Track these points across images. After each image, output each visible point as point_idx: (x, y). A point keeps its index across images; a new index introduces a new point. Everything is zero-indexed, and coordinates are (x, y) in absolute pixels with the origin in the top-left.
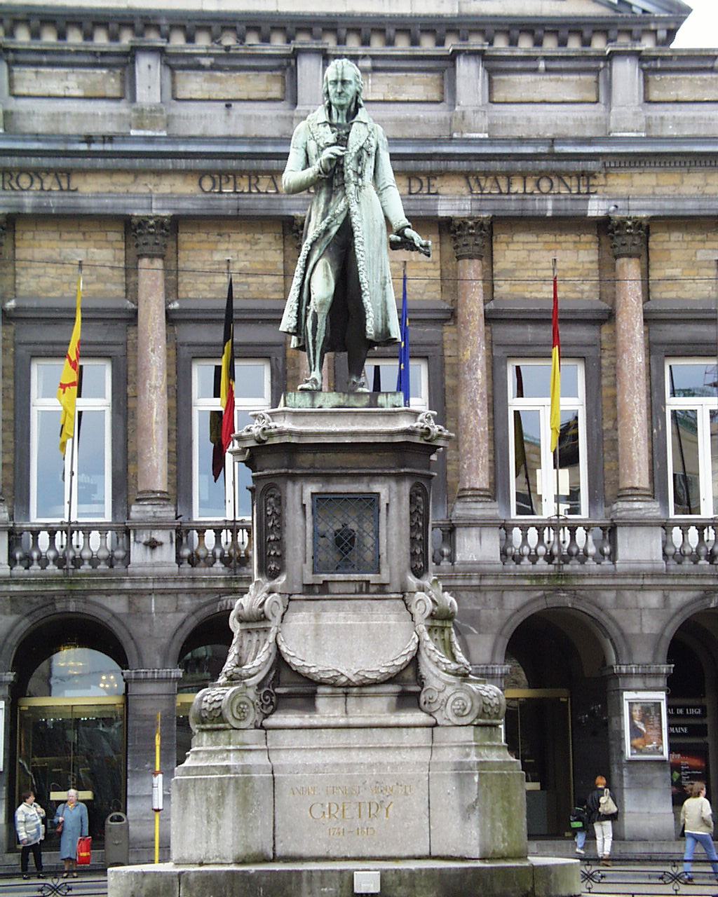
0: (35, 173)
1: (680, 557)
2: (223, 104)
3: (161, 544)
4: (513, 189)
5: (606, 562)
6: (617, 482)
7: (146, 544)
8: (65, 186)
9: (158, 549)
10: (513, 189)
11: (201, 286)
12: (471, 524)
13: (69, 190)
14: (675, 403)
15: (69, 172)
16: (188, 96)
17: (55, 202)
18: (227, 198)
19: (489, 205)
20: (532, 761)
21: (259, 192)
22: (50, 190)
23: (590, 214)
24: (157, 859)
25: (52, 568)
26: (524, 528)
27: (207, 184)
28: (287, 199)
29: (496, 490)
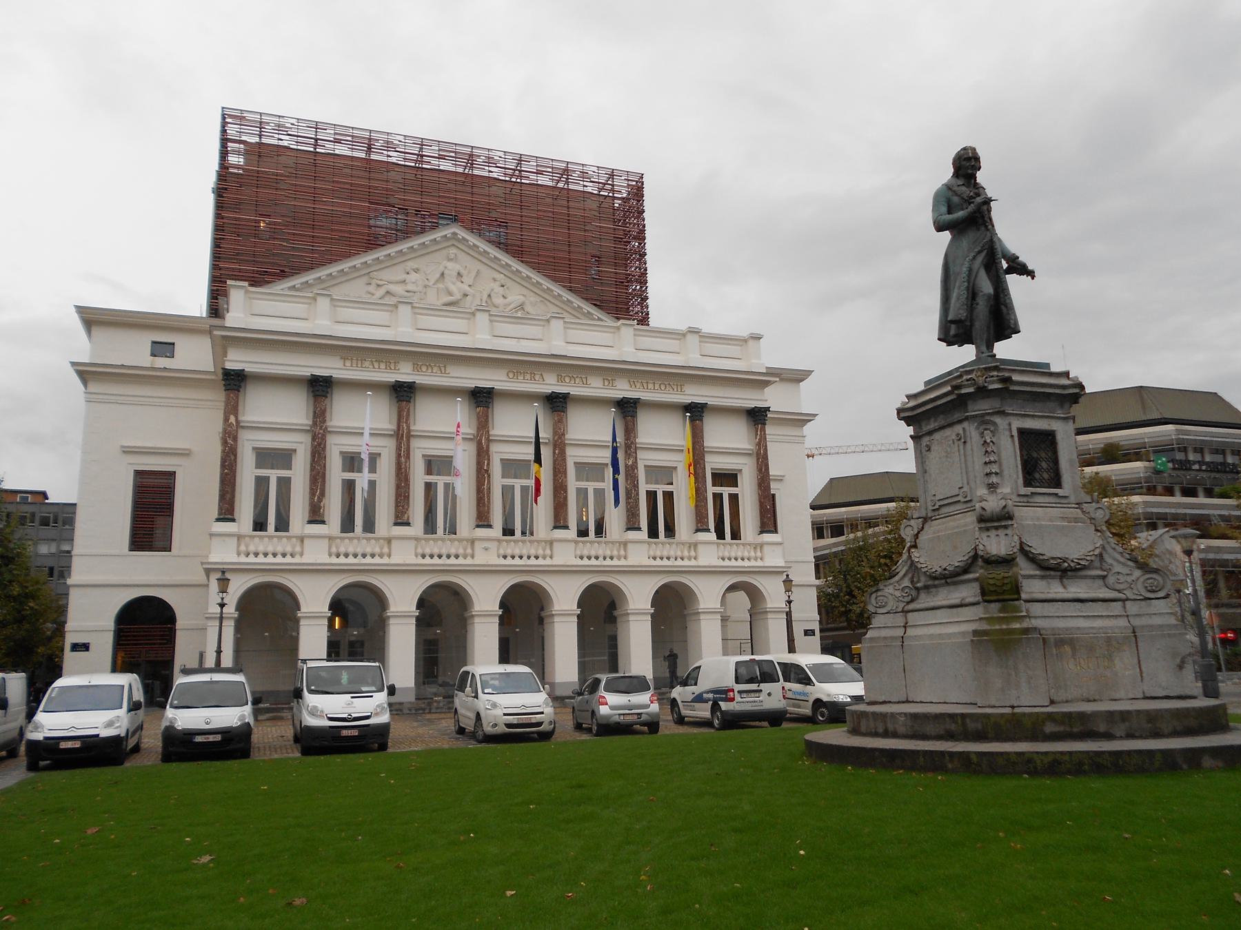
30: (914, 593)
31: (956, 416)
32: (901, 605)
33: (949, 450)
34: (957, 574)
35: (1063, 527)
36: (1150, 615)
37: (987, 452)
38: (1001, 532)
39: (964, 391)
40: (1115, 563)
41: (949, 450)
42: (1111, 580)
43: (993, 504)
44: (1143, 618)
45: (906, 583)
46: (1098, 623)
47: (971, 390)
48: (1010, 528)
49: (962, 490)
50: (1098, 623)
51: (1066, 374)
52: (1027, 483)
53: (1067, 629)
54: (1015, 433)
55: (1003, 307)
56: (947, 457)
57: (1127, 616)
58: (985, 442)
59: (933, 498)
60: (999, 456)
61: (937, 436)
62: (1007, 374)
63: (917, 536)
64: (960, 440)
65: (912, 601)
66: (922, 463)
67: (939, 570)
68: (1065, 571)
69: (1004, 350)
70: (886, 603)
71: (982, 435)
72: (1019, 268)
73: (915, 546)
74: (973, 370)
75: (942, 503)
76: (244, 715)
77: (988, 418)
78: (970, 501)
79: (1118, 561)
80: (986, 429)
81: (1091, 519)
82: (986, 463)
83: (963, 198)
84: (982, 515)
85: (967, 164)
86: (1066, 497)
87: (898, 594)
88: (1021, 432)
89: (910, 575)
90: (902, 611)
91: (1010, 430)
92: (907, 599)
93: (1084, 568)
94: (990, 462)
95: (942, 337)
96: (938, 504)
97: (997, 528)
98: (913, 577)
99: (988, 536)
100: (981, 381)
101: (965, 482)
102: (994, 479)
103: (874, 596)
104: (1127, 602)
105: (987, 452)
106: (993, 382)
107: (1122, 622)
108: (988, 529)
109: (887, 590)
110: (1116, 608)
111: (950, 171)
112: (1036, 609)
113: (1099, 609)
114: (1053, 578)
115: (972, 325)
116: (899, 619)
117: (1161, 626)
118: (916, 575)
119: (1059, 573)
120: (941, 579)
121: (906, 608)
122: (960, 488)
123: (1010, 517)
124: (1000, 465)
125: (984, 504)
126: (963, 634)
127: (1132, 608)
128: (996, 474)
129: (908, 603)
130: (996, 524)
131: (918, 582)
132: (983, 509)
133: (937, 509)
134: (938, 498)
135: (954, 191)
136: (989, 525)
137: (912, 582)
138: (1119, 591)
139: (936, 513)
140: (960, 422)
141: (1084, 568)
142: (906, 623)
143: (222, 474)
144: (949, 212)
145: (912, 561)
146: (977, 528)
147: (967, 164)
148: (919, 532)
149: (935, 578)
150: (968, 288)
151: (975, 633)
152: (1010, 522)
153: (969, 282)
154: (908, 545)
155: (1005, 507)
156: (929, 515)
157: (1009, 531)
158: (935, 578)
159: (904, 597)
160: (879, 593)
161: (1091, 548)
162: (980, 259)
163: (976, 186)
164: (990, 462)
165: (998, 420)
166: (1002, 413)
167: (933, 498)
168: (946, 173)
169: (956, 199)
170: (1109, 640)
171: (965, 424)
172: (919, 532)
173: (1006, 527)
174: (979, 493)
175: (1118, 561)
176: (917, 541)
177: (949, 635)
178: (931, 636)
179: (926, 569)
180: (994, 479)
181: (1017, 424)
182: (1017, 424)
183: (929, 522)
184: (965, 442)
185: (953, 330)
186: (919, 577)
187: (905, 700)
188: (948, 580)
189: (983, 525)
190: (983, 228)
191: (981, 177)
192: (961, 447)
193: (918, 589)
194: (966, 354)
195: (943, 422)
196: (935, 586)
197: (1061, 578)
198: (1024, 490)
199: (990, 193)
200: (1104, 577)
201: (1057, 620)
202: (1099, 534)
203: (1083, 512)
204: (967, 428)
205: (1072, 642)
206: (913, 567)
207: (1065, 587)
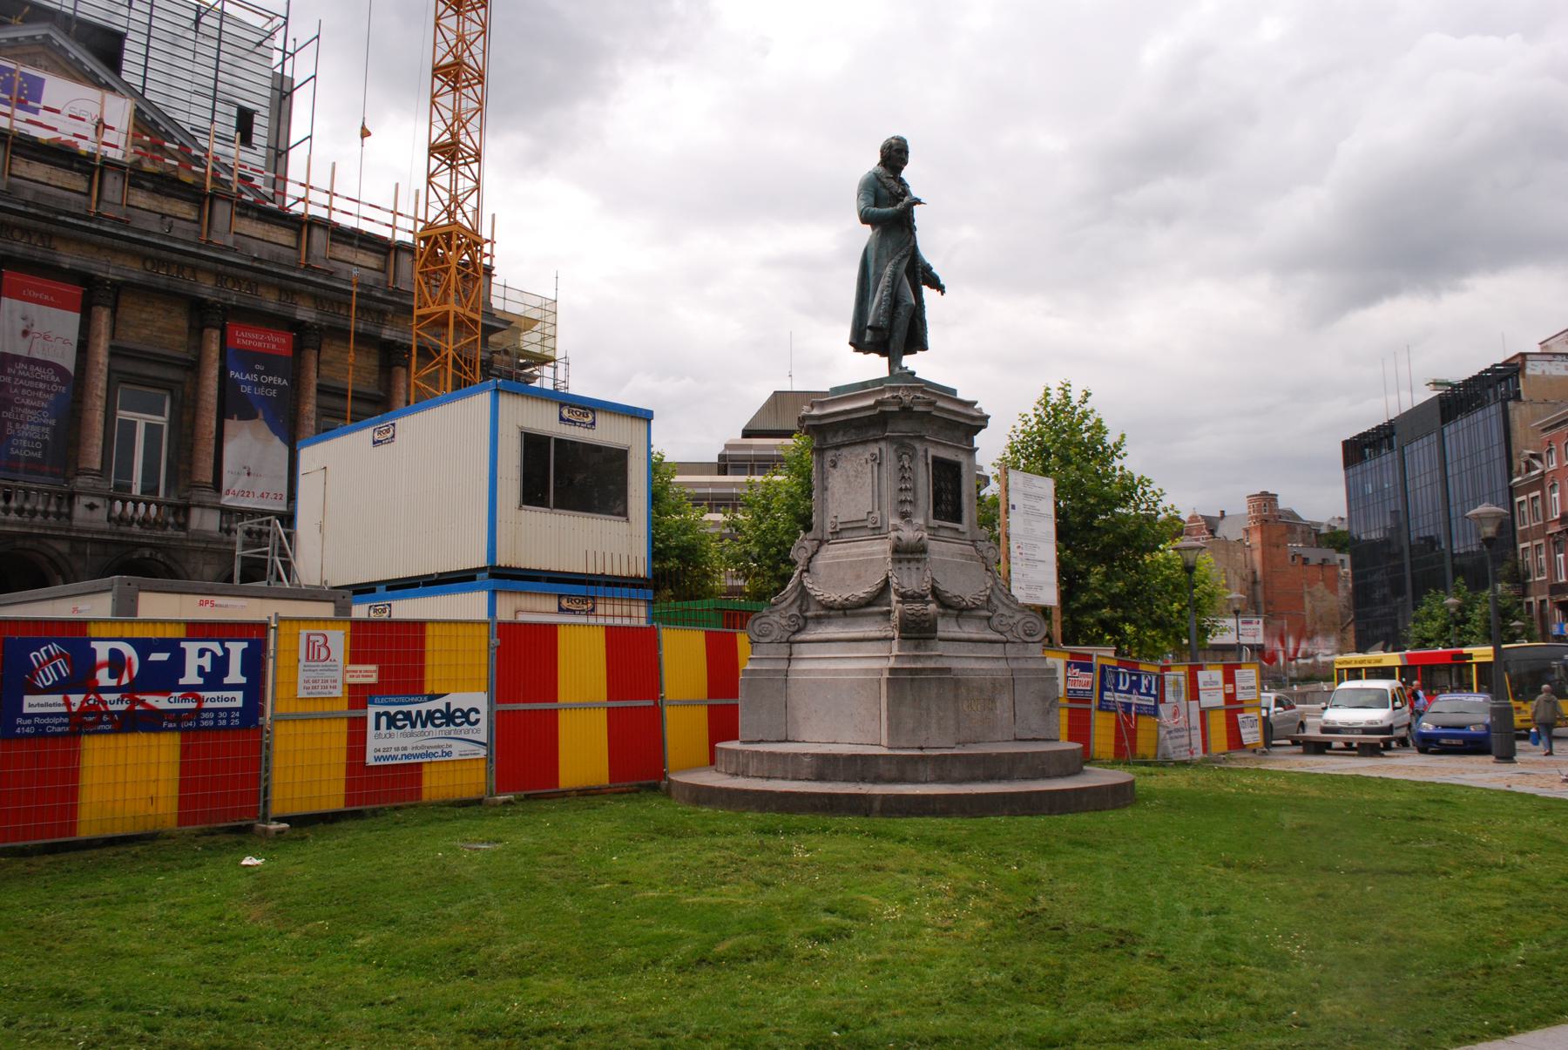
0: (26, 231)
1: (121, 520)
2: (159, 216)
3: (97, 507)
4: (342, 312)
5: (63, 519)
6: (77, 464)
7: (86, 506)
8: (47, 244)
9: (96, 510)
10: (342, 312)
11: (131, 334)
12: (201, 506)
13: (49, 248)
14: (123, 414)
15: (51, 236)
16: (18, 174)
17: (39, 254)
18: (162, 278)
19: (326, 318)
20: (1504, 646)
21: (184, 278)
22: (36, 245)
23: (383, 336)
24: (1397, 669)
25: (52, 519)
26: (148, 504)
27: (149, 265)
28: (1384, 512)
29: (104, 472)
30: (801, 622)
31: (871, 433)
32: (786, 635)
33: (860, 469)
34: (860, 606)
35: (963, 564)
36: (930, 657)
37: (903, 477)
38: (913, 565)
39: (887, 409)
40: (1000, 605)
41: (860, 469)
42: (995, 621)
43: (908, 534)
44: (1020, 661)
45: (794, 610)
46: (985, 665)
47: (896, 409)
48: (923, 562)
49: (871, 516)
50: (985, 665)
51: (972, 404)
52: (936, 515)
53: (963, 669)
54: (930, 461)
55: (917, 321)
56: (856, 476)
57: (1007, 659)
58: (903, 466)
59: (834, 520)
60: (915, 485)
61: (845, 452)
62: (933, 399)
63: (810, 560)
64: (874, 460)
65: (799, 631)
66: (823, 479)
67: (840, 599)
68: (962, 610)
69: (909, 362)
70: (771, 631)
71: (900, 458)
72: (936, 284)
73: (808, 571)
74: (899, 388)
75: (844, 526)
76: (1553, 673)
77: (907, 441)
78: (879, 528)
79: (1004, 604)
80: (904, 453)
81: (983, 557)
82: (901, 490)
83: (891, 193)
84: (897, 546)
85: (895, 155)
86: (964, 533)
87: (784, 622)
88: (936, 460)
89: (799, 603)
90: (787, 642)
91: (926, 458)
92: (792, 629)
93: (978, 608)
94: (906, 489)
95: (855, 341)
96: (839, 527)
97: (909, 561)
98: (801, 605)
99: (900, 568)
100: (907, 400)
101: (876, 507)
102: (908, 508)
103: (758, 622)
104: (1007, 645)
105: (903, 477)
106: (920, 404)
107: (1002, 665)
108: (900, 561)
109: (772, 617)
110: (998, 650)
111: (878, 159)
112: (949, 649)
113: (986, 651)
114: (950, 616)
115: (891, 336)
116: (784, 649)
117: (1036, 670)
118: (805, 603)
119: (956, 612)
120: (839, 609)
121: (792, 638)
122: (869, 513)
123: (924, 550)
124: (915, 494)
125: (899, 534)
126: (880, 671)
127: (1011, 650)
128: (910, 502)
129: (794, 633)
130: (909, 556)
131: (806, 610)
132: (899, 538)
133: (837, 533)
134: (840, 520)
135: (883, 182)
136: (902, 556)
137: (800, 610)
138: (1001, 633)
139: (835, 537)
140: (876, 441)
141: (978, 608)
142: (791, 655)
143: (1059, 559)
144: (876, 205)
145: (804, 588)
146: (889, 559)
147: (895, 155)
148: (812, 556)
149: (831, 608)
150: (891, 294)
151: (892, 671)
152: (923, 556)
153: (893, 287)
154: (800, 568)
155: (921, 539)
156: (826, 538)
157: (920, 565)
158: (831, 608)
159: (790, 626)
160: (764, 620)
161: (983, 588)
162: (904, 265)
163: (901, 182)
164: (906, 489)
165: (918, 446)
166: (921, 438)
167: (834, 520)
168: (871, 161)
169: (884, 192)
170: (994, 682)
171: (883, 445)
172: (812, 556)
173: (918, 560)
174: (892, 521)
175: (1004, 604)
176: (811, 565)
177: (847, 672)
178: (823, 672)
179: (821, 598)
180: (908, 508)
181: (932, 452)
182: (932, 452)
183: (826, 546)
184: (879, 464)
185: (868, 337)
186: (808, 604)
187: (784, 739)
188: (848, 612)
189: (897, 556)
190: (907, 230)
191: (906, 174)
192: (876, 468)
193: (806, 618)
194: (875, 366)
195: (854, 437)
196: (829, 617)
197: (957, 617)
198: (934, 523)
199: (915, 191)
200: (989, 618)
201: (955, 660)
202: (989, 574)
203: (977, 549)
204: (884, 450)
205: (957, 683)
206: (804, 594)
207: (960, 627)
